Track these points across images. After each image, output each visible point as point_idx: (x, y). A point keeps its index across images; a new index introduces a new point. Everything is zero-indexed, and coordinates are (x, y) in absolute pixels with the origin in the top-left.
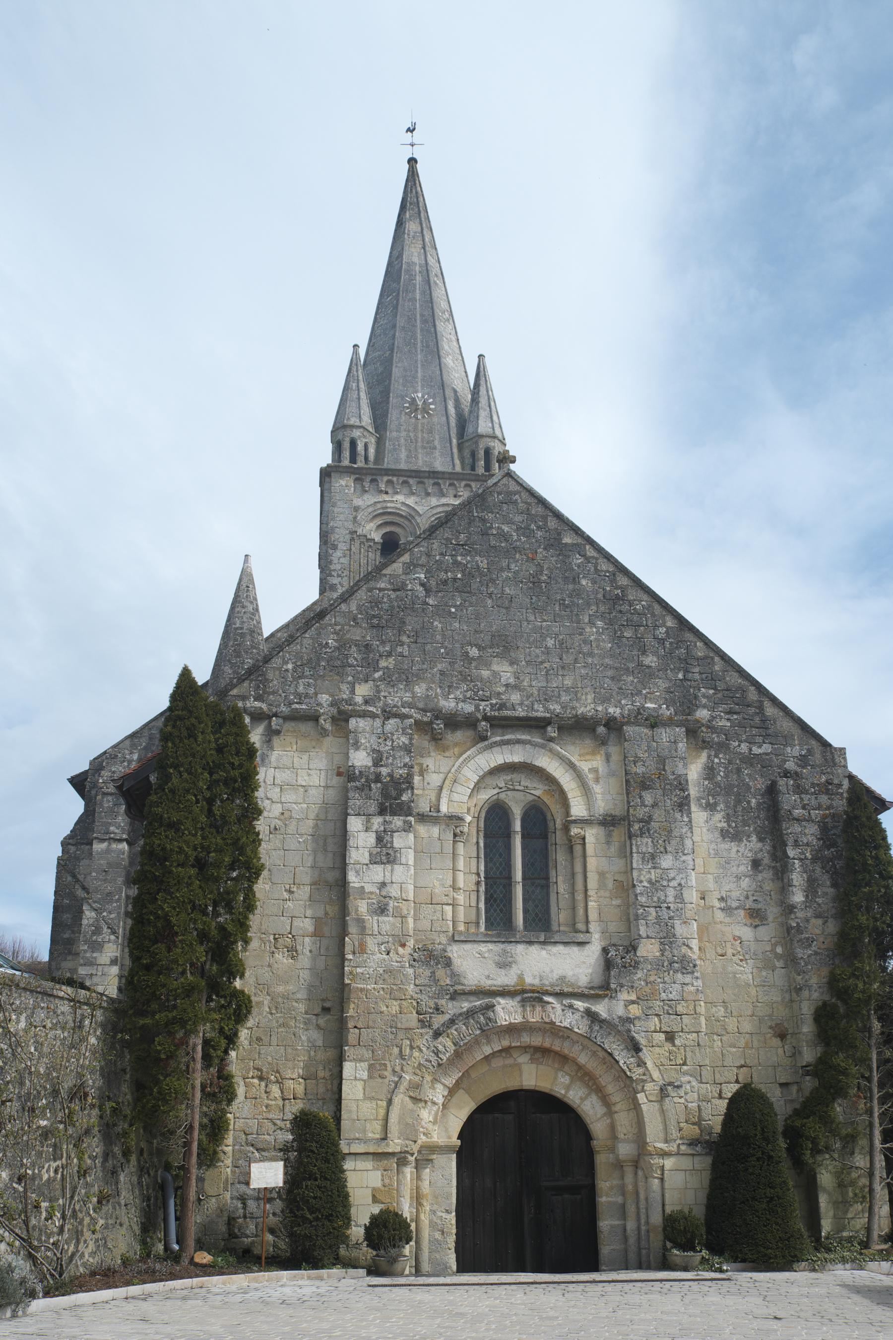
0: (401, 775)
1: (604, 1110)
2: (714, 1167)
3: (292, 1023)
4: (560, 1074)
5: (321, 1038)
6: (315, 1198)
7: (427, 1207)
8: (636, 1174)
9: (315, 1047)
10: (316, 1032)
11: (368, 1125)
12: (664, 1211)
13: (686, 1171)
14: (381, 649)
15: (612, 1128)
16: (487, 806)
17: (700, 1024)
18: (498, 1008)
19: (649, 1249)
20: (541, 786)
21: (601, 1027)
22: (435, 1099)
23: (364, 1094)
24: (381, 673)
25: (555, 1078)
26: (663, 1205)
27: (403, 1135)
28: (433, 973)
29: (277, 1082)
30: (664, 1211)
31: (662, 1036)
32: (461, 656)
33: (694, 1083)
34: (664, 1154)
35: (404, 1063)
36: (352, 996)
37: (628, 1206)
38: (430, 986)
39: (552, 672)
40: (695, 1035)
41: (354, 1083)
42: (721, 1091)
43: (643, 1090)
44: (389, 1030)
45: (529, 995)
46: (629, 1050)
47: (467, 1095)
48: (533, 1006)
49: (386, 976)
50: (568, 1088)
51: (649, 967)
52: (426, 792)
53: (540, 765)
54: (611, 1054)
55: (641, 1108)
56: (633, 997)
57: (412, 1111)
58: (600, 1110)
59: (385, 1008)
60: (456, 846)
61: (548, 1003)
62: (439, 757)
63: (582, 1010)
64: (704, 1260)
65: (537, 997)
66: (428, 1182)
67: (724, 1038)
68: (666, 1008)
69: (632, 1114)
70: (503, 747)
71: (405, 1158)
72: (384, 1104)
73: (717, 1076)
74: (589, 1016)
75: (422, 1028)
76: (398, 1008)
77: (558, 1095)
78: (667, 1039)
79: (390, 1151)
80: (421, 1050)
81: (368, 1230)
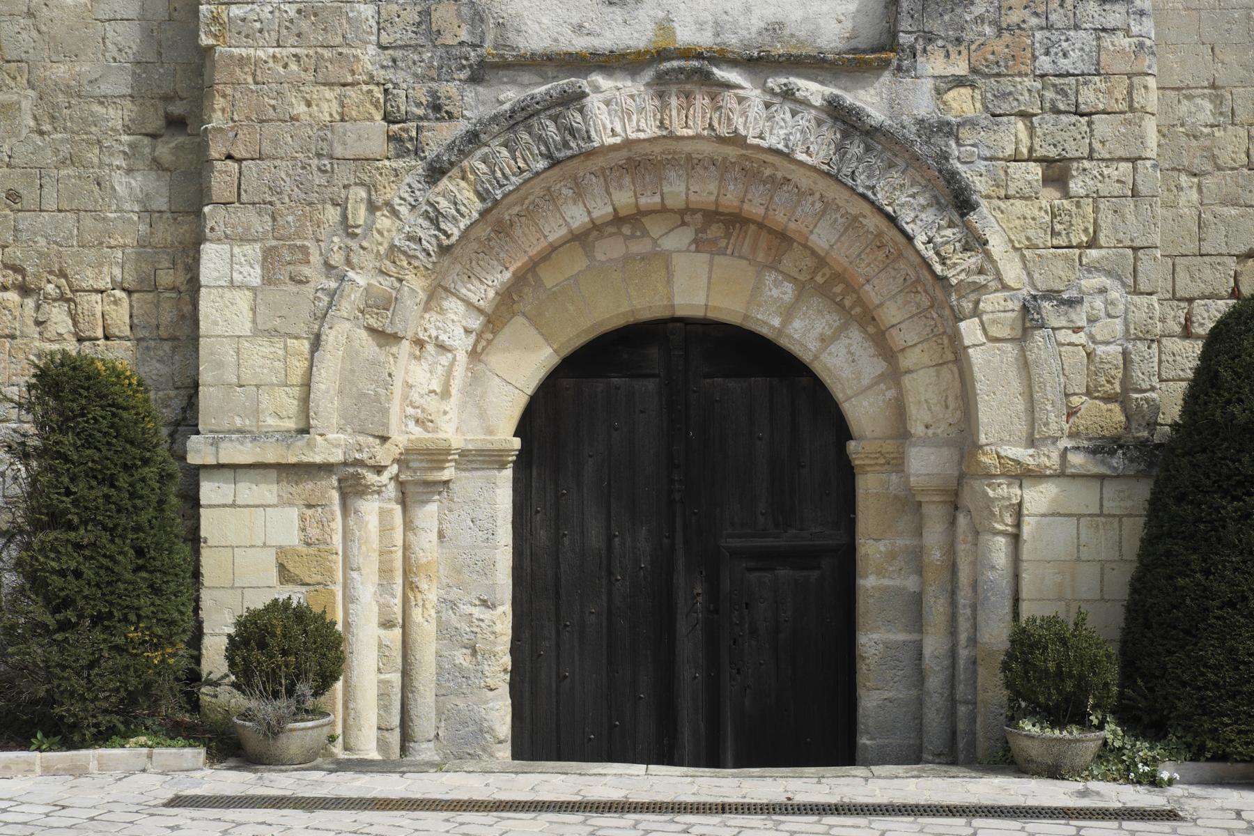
1: (880, 366)
2: (1155, 507)
3: (93, 155)
4: (770, 278)
5: (165, 191)
6: (62, 573)
7: (431, 592)
9: (151, 212)
10: (153, 175)
11: (264, 398)
12: (1016, 614)
13: (1079, 516)
15: (899, 410)
17: (1142, 139)
18: (594, 102)
19: (975, 703)
21: (868, 149)
22: (443, 337)
23: (254, 321)
25: (757, 289)
26: (1016, 601)
27: (350, 421)
29: (62, 298)
30: (1016, 614)
31: (1036, 171)
33: (1116, 294)
34: (1024, 475)
35: (353, 244)
36: (218, 77)
37: (929, 599)
38: (416, 48)
40: (1125, 167)
41: (228, 294)
42: (1188, 319)
43: (976, 312)
44: (315, 162)
45: (675, 64)
46: (941, 207)
47: (533, 331)
49: (304, 25)
50: (788, 313)
54: (892, 220)
55: (968, 357)
56: (961, 68)
57: (375, 363)
58: (871, 366)
59: (301, 109)
61: (728, 86)
63: (818, 102)
64: (1106, 752)
65: (696, 71)
66: (434, 536)
67: (1208, 181)
68: (1049, 94)
69: (949, 374)
71: (357, 477)
72: (305, 346)
73: (1183, 279)
74: (835, 119)
75: (398, 156)
76: (335, 106)
77: (764, 331)
78: (1047, 181)
79: (318, 459)
80: (395, 213)
81: (235, 645)
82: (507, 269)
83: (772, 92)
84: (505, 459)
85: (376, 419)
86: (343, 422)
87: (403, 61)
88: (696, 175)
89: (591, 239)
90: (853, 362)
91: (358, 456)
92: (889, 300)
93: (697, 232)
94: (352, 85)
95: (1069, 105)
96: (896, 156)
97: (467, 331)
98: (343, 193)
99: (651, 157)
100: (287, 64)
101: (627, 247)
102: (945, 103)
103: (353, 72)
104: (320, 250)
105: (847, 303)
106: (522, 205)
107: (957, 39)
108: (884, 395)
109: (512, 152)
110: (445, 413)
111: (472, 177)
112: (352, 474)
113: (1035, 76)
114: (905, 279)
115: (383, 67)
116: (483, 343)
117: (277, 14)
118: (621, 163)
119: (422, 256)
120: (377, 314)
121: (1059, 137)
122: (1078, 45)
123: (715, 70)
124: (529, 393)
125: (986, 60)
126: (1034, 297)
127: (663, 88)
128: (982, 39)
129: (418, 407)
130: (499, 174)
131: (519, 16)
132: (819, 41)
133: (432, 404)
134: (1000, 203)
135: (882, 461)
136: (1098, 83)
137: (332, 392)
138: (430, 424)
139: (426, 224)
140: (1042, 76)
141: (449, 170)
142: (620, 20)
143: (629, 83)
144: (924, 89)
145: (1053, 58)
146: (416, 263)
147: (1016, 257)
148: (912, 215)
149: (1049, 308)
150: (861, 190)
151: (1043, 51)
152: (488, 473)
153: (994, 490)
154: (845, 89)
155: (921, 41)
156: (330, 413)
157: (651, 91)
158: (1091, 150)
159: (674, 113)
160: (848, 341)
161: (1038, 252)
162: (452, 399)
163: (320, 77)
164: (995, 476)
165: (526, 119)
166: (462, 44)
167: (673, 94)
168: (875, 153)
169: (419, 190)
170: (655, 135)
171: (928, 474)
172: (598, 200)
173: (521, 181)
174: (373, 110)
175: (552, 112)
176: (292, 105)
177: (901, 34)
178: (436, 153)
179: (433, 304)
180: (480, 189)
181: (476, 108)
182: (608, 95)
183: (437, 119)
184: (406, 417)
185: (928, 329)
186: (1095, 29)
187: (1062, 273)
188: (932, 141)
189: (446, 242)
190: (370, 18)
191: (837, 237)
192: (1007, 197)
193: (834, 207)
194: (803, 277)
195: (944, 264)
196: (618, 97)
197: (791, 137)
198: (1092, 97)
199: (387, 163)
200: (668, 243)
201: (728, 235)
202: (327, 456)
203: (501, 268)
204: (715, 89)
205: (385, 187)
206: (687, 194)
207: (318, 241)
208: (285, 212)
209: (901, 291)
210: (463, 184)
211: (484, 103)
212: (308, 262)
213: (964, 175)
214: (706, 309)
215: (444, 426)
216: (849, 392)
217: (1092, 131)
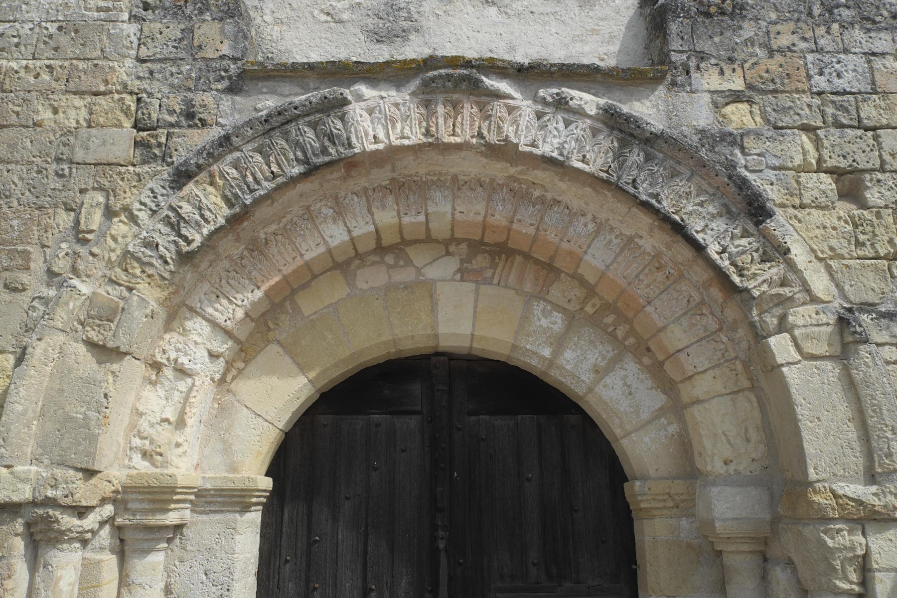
1: (658, 400)
4: (538, 308)
8: (764, 577)
18: (356, 110)
21: (648, 158)
22: (183, 360)
25: (525, 318)
35: (83, 250)
38: (174, 61)
43: (783, 326)
47: (287, 360)
48: (456, 106)
49: (63, 40)
50: (559, 343)
51: (773, 16)
54: (679, 230)
55: (782, 377)
56: (738, 84)
57: (90, 382)
59: (46, 115)
61: (497, 95)
65: (463, 78)
68: (830, 110)
69: (747, 404)
71: (48, 521)
75: (144, 162)
76: (83, 114)
80: (133, 219)
82: (258, 288)
83: (544, 101)
84: (247, 500)
85: (81, 448)
86: (40, 451)
87: (160, 72)
88: (463, 195)
89: (353, 267)
90: (630, 394)
91: (50, 493)
92: (673, 322)
93: (462, 261)
94: (103, 94)
95: (851, 119)
96: (679, 163)
97: (213, 356)
98: (78, 198)
99: (416, 178)
100: (38, 74)
101: (390, 277)
102: (724, 116)
103: (106, 82)
104: (45, 257)
105: (620, 333)
106: (279, 224)
107: (729, 59)
108: (666, 430)
109: (266, 157)
110: (178, 445)
111: (220, 182)
112: (42, 517)
113: (812, 93)
114: (688, 301)
115: (139, 78)
116: (234, 372)
117: (37, 30)
118: (384, 183)
119: (157, 263)
120: (99, 326)
121: (848, 148)
122: (851, 67)
123: (484, 78)
124: (281, 425)
125: (761, 77)
126: (850, 310)
127: (429, 97)
128: (755, 59)
129: (146, 438)
130: (250, 179)
133: (164, 434)
134: (796, 212)
135: (671, 504)
136: (877, 101)
137: (30, 414)
138: (159, 458)
139: (166, 230)
140: (820, 94)
141: (196, 175)
143: (393, 93)
144: (702, 102)
145: (828, 77)
146: (150, 271)
147: (821, 267)
148: (702, 224)
149: (869, 321)
150: (644, 198)
151: (816, 71)
152: (228, 516)
153: (832, 538)
154: (620, 101)
155: (693, 59)
156: (23, 440)
157: (417, 100)
158: (883, 162)
159: (441, 121)
160: (623, 373)
161: (845, 262)
162: (188, 430)
163: (71, 86)
164: (832, 520)
165: (283, 124)
166: (222, 57)
167: (440, 102)
168: (657, 161)
169: (163, 195)
170: (421, 142)
171: (737, 519)
172: (360, 219)
173: (273, 186)
174: (122, 117)
175: (312, 118)
176: (37, 112)
177: (672, 53)
178: (184, 158)
179: (175, 324)
180: (229, 194)
181: (232, 115)
182: (371, 103)
183: (190, 126)
184: (131, 449)
185: (719, 353)
186: (864, 53)
187: (873, 285)
188: (716, 149)
189: (185, 248)
190: (132, 35)
191: (613, 256)
192: (802, 206)
193: (608, 228)
194: (573, 307)
195: (741, 275)
196: (382, 105)
197: (566, 146)
198: (874, 113)
199: (131, 168)
200: (432, 273)
201: (494, 266)
202: (10, 493)
203: (252, 287)
204: (484, 99)
205: (125, 192)
206: (453, 214)
207: (43, 246)
208: (11, 216)
209: (685, 313)
210: (210, 189)
211: (240, 112)
212: (28, 268)
213: (754, 183)
214: (472, 339)
215: (176, 460)
216: (628, 427)
217: (879, 144)
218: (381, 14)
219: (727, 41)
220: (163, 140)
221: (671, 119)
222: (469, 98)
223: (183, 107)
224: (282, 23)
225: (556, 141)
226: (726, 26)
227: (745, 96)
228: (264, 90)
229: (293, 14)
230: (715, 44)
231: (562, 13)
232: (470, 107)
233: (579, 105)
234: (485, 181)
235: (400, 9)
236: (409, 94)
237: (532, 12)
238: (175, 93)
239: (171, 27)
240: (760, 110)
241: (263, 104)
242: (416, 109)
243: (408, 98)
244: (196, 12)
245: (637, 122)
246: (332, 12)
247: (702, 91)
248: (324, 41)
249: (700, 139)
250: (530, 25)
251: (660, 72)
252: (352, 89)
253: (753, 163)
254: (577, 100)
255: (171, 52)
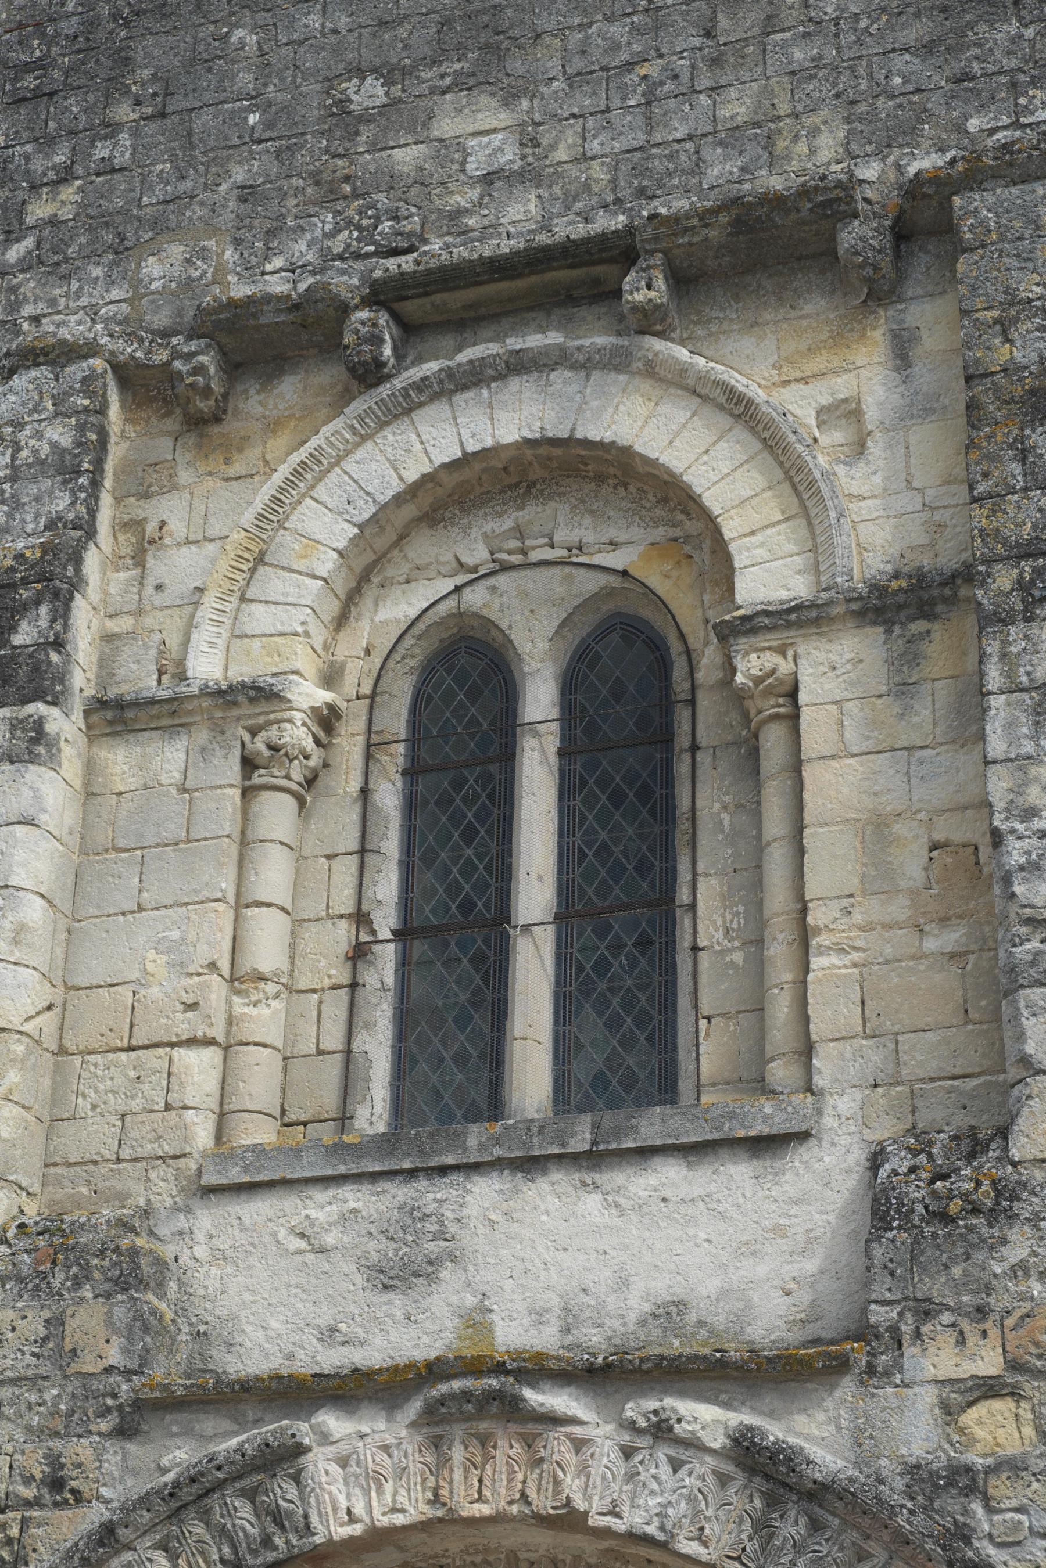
0: (20, 557)
14: (38, 165)
16: (416, 652)
20: (636, 532)
21: (816, 1526)
24: (29, 242)
28: (56, 1322)
32: (321, 120)
38: (34, 1381)
39: (669, 86)
45: (456, 1385)
48: (485, 1440)
52: (148, 621)
53: (608, 436)
60: (255, 807)
61: (554, 1420)
62: (210, 483)
70: (459, 399)
83: (632, 1426)
102: (962, 1431)
107: (979, 1309)
123: (528, 1393)
127: (438, 1430)
131: (233, 1317)
132: (749, 1330)
142: (399, 1315)
144: (919, 1406)
155: (909, 1317)
157: (419, 1438)
159: (458, 1475)
165: (200, 1497)
166: (109, 1370)
170: (423, 1518)
175: (247, 1482)
177: (873, 1306)
182: (343, 1448)
183: (56, 1505)
188: (936, 1505)
196: (361, 1450)
204: (532, 1428)
211: (135, 1473)
218: (391, 1230)
219: (976, 1272)
220: (14, 1532)
221: (860, 1445)
222: (506, 1428)
223: (47, 1469)
224: (225, 1259)
225: (653, 1502)
226: (976, 1240)
227: (1006, 1385)
228: (175, 1429)
229: (243, 1239)
230: (954, 1280)
231: (720, 1196)
232: (507, 1445)
233: (692, 1433)
234: (563, 1561)
235: (426, 1217)
236: (407, 1426)
237: (664, 1200)
238: (34, 1442)
239: (30, 1317)
240: (1033, 1411)
241: (171, 1457)
242: (417, 1455)
243: (404, 1433)
244: (69, 1284)
245: (791, 1460)
246: (309, 1232)
247: (924, 1382)
248: (294, 1291)
249: (908, 1486)
250: (659, 1227)
251: (834, 1359)
252: (313, 1421)
253: (1002, 1529)
254: (689, 1422)
255: (28, 1365)
